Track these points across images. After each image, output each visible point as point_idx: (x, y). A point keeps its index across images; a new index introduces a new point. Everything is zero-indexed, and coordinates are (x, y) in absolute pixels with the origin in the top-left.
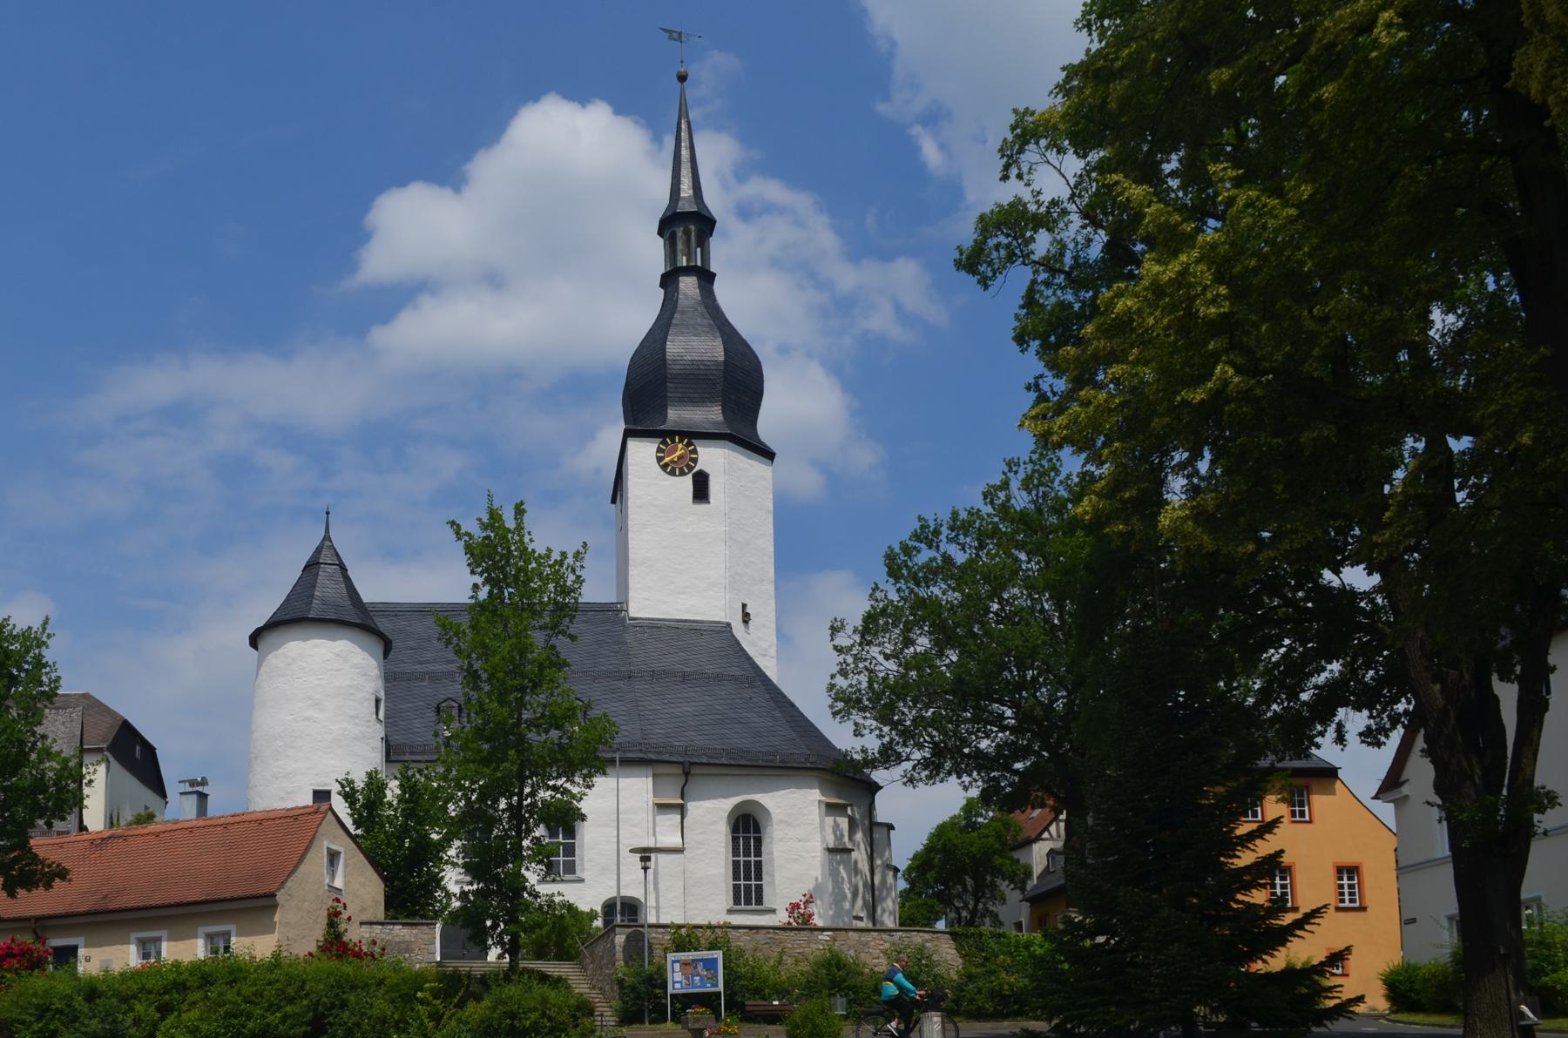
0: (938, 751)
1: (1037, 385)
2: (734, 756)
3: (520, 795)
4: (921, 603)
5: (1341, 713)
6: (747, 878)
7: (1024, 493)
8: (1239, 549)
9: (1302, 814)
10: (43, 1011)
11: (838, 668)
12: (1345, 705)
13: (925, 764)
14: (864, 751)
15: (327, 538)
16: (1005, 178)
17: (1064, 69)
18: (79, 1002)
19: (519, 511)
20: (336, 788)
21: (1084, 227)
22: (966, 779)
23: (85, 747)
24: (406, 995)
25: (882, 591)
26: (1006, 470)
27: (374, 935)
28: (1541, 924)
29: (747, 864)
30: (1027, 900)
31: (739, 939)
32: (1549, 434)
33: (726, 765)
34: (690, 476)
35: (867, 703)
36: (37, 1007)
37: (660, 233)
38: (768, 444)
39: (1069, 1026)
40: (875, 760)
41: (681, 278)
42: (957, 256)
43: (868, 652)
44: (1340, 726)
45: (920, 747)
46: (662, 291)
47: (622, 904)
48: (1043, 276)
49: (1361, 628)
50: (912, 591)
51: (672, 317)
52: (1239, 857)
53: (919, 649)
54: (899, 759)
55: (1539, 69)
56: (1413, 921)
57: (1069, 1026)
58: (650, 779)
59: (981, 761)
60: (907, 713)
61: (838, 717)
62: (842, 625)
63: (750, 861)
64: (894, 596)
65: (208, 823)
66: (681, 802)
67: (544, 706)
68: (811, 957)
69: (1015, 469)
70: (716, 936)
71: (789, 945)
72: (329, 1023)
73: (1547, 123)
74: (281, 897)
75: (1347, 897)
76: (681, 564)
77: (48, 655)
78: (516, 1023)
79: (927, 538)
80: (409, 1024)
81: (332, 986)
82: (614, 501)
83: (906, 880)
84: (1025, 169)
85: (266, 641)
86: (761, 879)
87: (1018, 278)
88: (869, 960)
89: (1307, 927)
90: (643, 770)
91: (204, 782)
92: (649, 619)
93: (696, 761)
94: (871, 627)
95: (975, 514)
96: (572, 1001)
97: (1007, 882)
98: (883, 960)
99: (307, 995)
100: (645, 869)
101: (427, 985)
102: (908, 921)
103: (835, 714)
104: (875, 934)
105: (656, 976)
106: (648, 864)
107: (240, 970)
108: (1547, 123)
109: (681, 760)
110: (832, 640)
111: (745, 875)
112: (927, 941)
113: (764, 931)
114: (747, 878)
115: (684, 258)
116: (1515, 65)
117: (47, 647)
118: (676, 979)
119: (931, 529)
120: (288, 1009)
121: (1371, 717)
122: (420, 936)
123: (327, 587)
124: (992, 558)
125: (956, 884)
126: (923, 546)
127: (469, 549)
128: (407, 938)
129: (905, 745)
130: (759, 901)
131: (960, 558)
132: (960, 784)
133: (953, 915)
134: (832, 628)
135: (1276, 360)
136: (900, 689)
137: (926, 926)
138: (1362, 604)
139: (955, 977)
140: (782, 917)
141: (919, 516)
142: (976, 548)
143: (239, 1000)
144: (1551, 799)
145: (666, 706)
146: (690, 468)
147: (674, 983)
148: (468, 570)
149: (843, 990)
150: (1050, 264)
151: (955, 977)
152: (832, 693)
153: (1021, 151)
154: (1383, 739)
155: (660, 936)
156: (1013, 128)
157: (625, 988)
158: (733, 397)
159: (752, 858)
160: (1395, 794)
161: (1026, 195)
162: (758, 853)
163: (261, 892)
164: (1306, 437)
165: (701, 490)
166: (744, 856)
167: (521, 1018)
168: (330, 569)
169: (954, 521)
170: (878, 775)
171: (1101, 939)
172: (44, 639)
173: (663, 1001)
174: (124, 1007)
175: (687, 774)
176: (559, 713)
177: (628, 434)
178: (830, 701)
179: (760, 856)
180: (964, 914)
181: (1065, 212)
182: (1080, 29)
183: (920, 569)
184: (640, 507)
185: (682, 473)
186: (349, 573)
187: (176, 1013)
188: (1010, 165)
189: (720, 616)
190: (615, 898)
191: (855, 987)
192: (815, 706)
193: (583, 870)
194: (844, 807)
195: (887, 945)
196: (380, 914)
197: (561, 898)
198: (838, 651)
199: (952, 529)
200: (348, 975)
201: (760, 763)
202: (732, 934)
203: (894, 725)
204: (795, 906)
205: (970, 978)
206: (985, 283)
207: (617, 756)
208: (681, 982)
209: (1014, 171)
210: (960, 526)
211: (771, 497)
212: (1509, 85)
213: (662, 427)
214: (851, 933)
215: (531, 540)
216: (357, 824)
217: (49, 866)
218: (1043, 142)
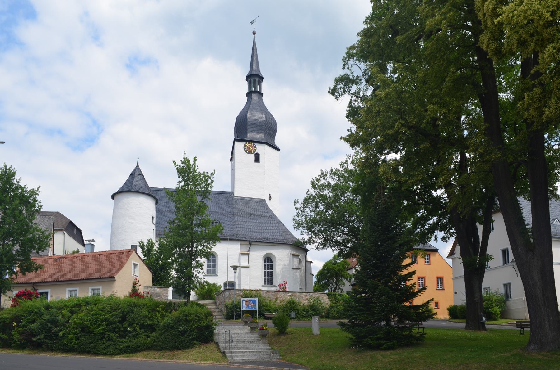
0: (325, 240)
1: (351, 130)
3: (192, 247)
4: (321, 196)
5: (436, 232)
7: (352, 165)
8: (402, 179)
9: (428, 262)
10: (30, 313)
11: (296, 214)
12: (437, 229)
13: (322, 244)
14: (303, 239)
15: (138, 166)
16: (344, 68)
17: (358, 34)
18: (43, 310)
19: (195, 159)
20: (138, 244)
21: (366, 85)
22: (333, 248)
23: (55, 229)
24: (153, 309)
26: (347, 158)
27: (148, 291)
28: (490, 295)
29: (268, 272)
30: (351, 285)
32: (488, 149)
33: (256, 242)
34: (254, 154)
35: (305, 225)
36: (29, 311)
37: (247, 80)
38: (278, 146)
39: (353, 321)
40: (307, 242)
42: (329, 90)
43: (305, 210)
44: (436, 236)
45: (320, 238)
46: (247, 98)
47: (229, 283)
48: (354, 98)
49: (442, 208)
50: (319, 192)
52: (403, 271)
53: (320, 210)
54: (314, 242)
55: (486, 41)
56: (456, 293)
57: (353, 321)
58: (239, 245)
59: (337, 243)
60: (316, 228)
61: (296, 229)
64: (313, 194)
65: (94, 254)
67: (200, 220)
68: (285, 300)
69: (349, 158)
70: (257, 293)
72: (127, 317)
73: (488, 57)
74: (117, 277)
75: (439, 286)
77: (38, 198)
78: (187, 318)
79: (323, 176)
80: (153, 318)
81: (129, 306)
82: (231, 161)
83: (316, 278)
84: (350, 66)
85: (117, 197)
87: (346, 99)
88: (303, 302)
89: (422, 292)
91: (93, 241)
93: (253, 240)
94: (306, 201)
95: (337, 170)
96: (206, 312)
97: (345, 280)
98: (307, 302)
99: (120, 308)
100: (235, 272)
101: (160, 306)
102: (316, 290)
103: (295, 228)
105: (237, 305)
106: (236, 271)
107: (99, 300)
108: (488, 57)
109: (249, 240)
112: (320, 296)
113: (271, 292)
115: (254, 88)
116: (480, 40)
117: (38, 195)
118: (244, 306)
119: (324, 174)
120: (114, 313)
121: (445, 233)
122: (163, 291)
123: (137, 181)
124: (342, 183)
125: (331, 280)
126: (322, 179)
127: (177, 169)
128: (159, 292)
129: (315, 238)
130: (272, 283)
131: (333, 183)
132: (332, 250)
133: (330, 289)
135: (414, 123)
136: (314, 221)
137: (322, 292)
138: (442, 201)
139: (328, 307)
140: (278, 288)
142: (338, 180)
143: (97, 310)
144: (491, 258)
146: (254, 152)
147: (243, 307)
148: (178, 176)
149: (294, 310)
150: (356, 95)
151: (328, 307)
152: (294, 222)
153: (348, 61)
154: (447, 240)
156: (346, 54)
159: (270, 270)
160: (452, 257)
161: (349, 73)
162: (272, 269)
163: (110, 276)
164: (422, 146)
165: (257, 159)
167: (189, 317)
168: (138, 176)
170: (308, 247)
171: (363, 295)
172: (37, 192)
173: (240, 313)
174: (58, 312)
175: (250, 244)
176: (204, 221)
177: (235, 140)
178: (293, 224)
180: (333, 289)
181: (361, 80)
182: (365, 24)
183: (321, 185)
185: (252, 153)
186: (145, 177)
187: (76, 314)
188: (345, 64)
189: (262, 197)
190: (226, 282)
191: (298, 309)
192: (289, 225)
193: (218, 273)
194: (298, 256)
195: (308, 297)
196: (151, 284)
197: (204, 280)
199: (331, 174)
200: (134, 302)
203: (312, 232)
204: (281, 285)
205: (332, 307)
206: (337, 98)
207: (228, 238)
209: (346, 66)
210: (333, 173)
212: (478, 45)
213: (246, 139)
214: (297, 293)
215: (198, 169)
216: (145, 256)
217: (36, 265)
218: (355, 58)
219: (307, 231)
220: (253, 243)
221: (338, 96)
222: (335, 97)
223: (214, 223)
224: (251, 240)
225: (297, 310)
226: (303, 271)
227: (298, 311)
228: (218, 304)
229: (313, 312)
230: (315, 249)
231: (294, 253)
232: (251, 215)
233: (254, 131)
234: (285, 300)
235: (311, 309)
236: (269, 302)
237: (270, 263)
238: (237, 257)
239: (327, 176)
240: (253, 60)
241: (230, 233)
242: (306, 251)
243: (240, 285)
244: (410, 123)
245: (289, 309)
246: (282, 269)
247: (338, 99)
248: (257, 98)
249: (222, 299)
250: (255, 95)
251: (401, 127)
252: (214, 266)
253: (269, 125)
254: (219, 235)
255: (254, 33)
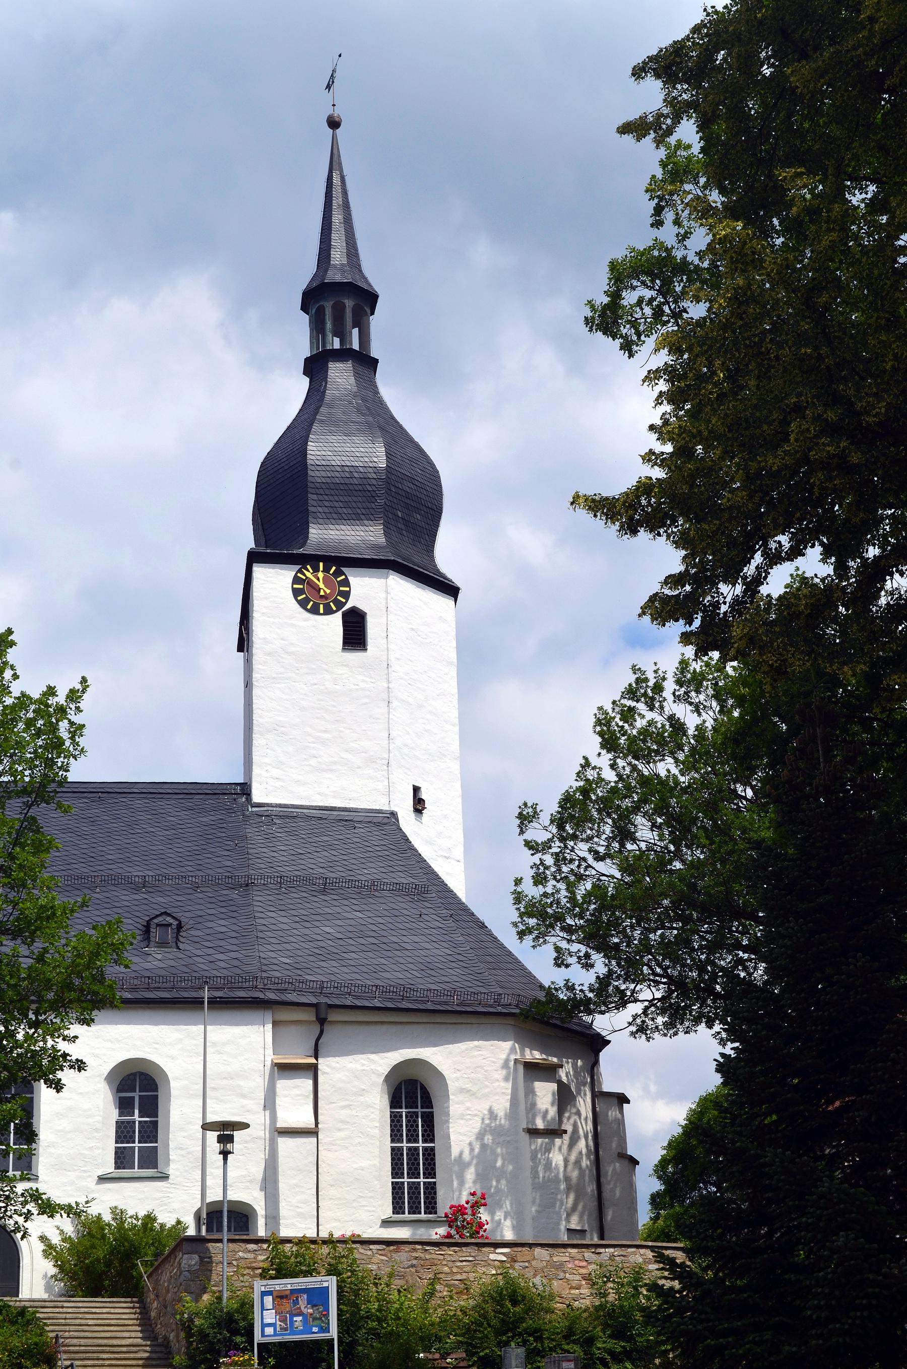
2: (391, 995)
6: (414, 1173)
13: (664, 1006)
14: (570, 988)
16: (658, 224)
25: (594, 768)
29: (413, 1152)
31: (369, 1260)
37: (305, 308)
38: (450, 575)
41: (331, 365)
43: (573, 850)
46: (306, 381)
51: (317, 411)
54: (623, 1002)
58: (269, 1027)
62: (535, 812)
63: (417, 1149)
64: (610, 776)
66: (313, 1061)
71: (446, 1269)
76: (326, 731)
79: (645, 695)
82: (240, 648)
83: (659, 1178)
86: (433, 1175)
90: (258, 1014)
92: (280, 806)
93: (337, 1002)
98: (585, 1291)
104: (573, 1251)
109: (315, 1001)
110: (522, 832)
111: (409, 1169)
113: (407, 1248)
114: (414, 1173)
118: (268, 1320)
119: (651, 683)
126: (641, 707)
134: (521, 816)
141: (634, 666)
145: (297, 925)
147: (264, 1326)
149: (520, 1334)
155: (250, 1256)
157: (192, 1336)
158: (400, 514)
159: (421, 1144)
162: (429, 1136)
166: (409, 1141)
169: (682, 672)
170: (602, 1023)
175: (322, 1021)
177: (253, 558)
179: (432, 1141)
184: (269, 654)
185: (328, 611)
188: (663, 208)
189: (381, 804)
191: (536, 1330)
193: (168, 1162)
195: (592, 1267)
198: (531, 848)
199: (679, 683)
201: (430, 1006)
202: (360, 1252)
208: (273, 1325)
211: (454, 644)
214: (538, 1251)
215: (15, 677)
219: (583, 949)
220: (333, 1016)
221: (635, 338)
222: (618, 342)
223: (153, 926)
224: (323, 1000)
225: (537, 1334)
226: (582, 1144)
227: (539, 1339)
228: (153, 1314)
229: (618, 1346)
230: (633, 1034)
231: (536, 1056)
232: (326, 887)
233: (337, 516)
234: (475, 1289)
235: (606, 1326)
236: (394, 1296)
237: (419, 1110)
238: (258, 1084)
239: (664, 694)
240: (330, 229)
241: (226, 973)
242: (598, 1043)
243: (273, 1218)
244: (868, 413)
245: (499, 1333)
246: (480, 1136)
247: (635, 348)
248: (352, 380)
249: (168, 1292)
250: (339, 365)
251: (816, 436)
252: (151, 1132)
253: (407, 486)
254: (113, 971)
255: (334, 124)
